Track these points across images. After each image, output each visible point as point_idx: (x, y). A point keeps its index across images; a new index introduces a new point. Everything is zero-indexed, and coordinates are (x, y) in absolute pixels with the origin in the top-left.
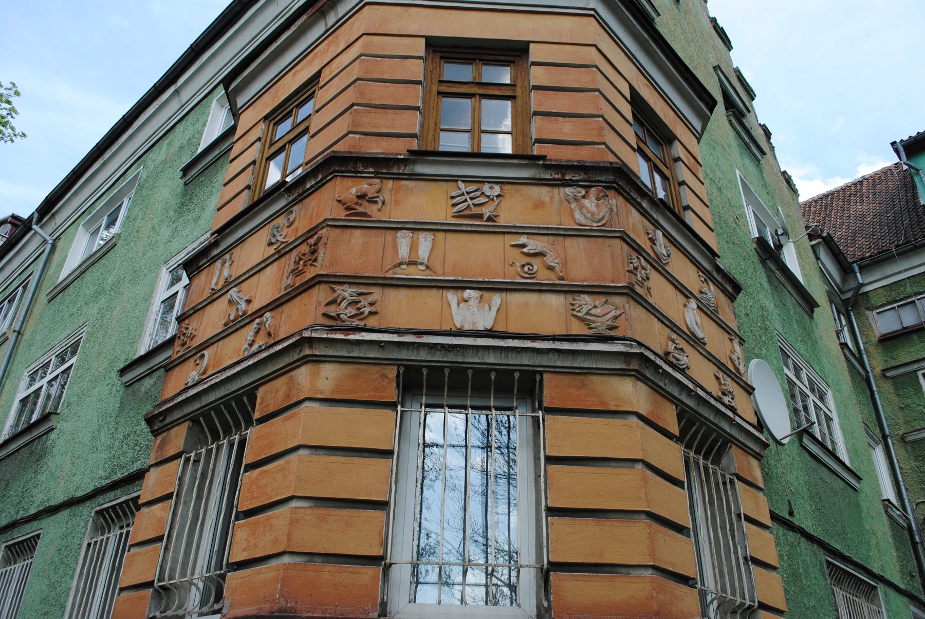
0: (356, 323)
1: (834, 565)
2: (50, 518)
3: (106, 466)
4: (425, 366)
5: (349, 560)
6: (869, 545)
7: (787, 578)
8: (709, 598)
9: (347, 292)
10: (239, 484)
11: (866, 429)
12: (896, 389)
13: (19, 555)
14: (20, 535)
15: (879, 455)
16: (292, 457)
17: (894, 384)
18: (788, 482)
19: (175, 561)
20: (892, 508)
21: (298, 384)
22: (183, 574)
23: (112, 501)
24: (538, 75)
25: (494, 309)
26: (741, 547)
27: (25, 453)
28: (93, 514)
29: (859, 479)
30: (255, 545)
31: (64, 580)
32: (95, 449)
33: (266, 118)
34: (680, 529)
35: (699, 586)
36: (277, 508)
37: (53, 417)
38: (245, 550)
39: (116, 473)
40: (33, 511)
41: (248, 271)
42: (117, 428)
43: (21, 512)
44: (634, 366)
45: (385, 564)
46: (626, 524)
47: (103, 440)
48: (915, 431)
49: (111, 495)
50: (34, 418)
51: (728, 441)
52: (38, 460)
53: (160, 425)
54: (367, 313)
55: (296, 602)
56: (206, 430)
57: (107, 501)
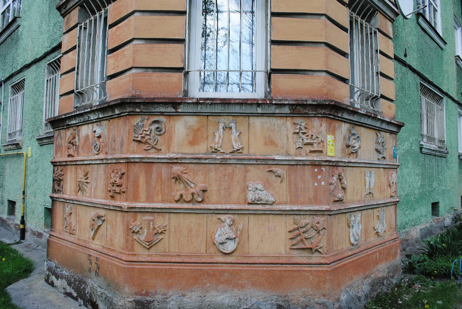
1: (424, 85)
2: (27, 70)
3: (48, 41)
5: (166, 70)
6: (444, 77)
8: (356, 90)
10: (107, 36)
11: (454, 18)
13: (19, 91)
14: (16, 79)
16: (132, 18)
18: (407, 41)
19: (82, 80)
20: (459, 60)
22: (87, 85)
23: (54, 58)
26: (376, 67)
27: (9, 40)
28: (46, 66)
29: (445, 43)
30: (118, 66)
31: (39, 98)
32: (41, 33)
34: (344, 54)
35: (350, 83)
36: (127, 45)
37: (18, 19)
38: (113, 69)
39: (53, 44)
40: (19, 68)
42: (50, 21)
43: (14, 69)
45: (185, 72)
46: (314, 49)
47: (44, 28)
49: (53, 55)
50: (10, 21)
51: (376, 10)
52: (16, 43)
53: (65, 10)
55: (141, 92)
56: (88, 10)
57: (52, 58)
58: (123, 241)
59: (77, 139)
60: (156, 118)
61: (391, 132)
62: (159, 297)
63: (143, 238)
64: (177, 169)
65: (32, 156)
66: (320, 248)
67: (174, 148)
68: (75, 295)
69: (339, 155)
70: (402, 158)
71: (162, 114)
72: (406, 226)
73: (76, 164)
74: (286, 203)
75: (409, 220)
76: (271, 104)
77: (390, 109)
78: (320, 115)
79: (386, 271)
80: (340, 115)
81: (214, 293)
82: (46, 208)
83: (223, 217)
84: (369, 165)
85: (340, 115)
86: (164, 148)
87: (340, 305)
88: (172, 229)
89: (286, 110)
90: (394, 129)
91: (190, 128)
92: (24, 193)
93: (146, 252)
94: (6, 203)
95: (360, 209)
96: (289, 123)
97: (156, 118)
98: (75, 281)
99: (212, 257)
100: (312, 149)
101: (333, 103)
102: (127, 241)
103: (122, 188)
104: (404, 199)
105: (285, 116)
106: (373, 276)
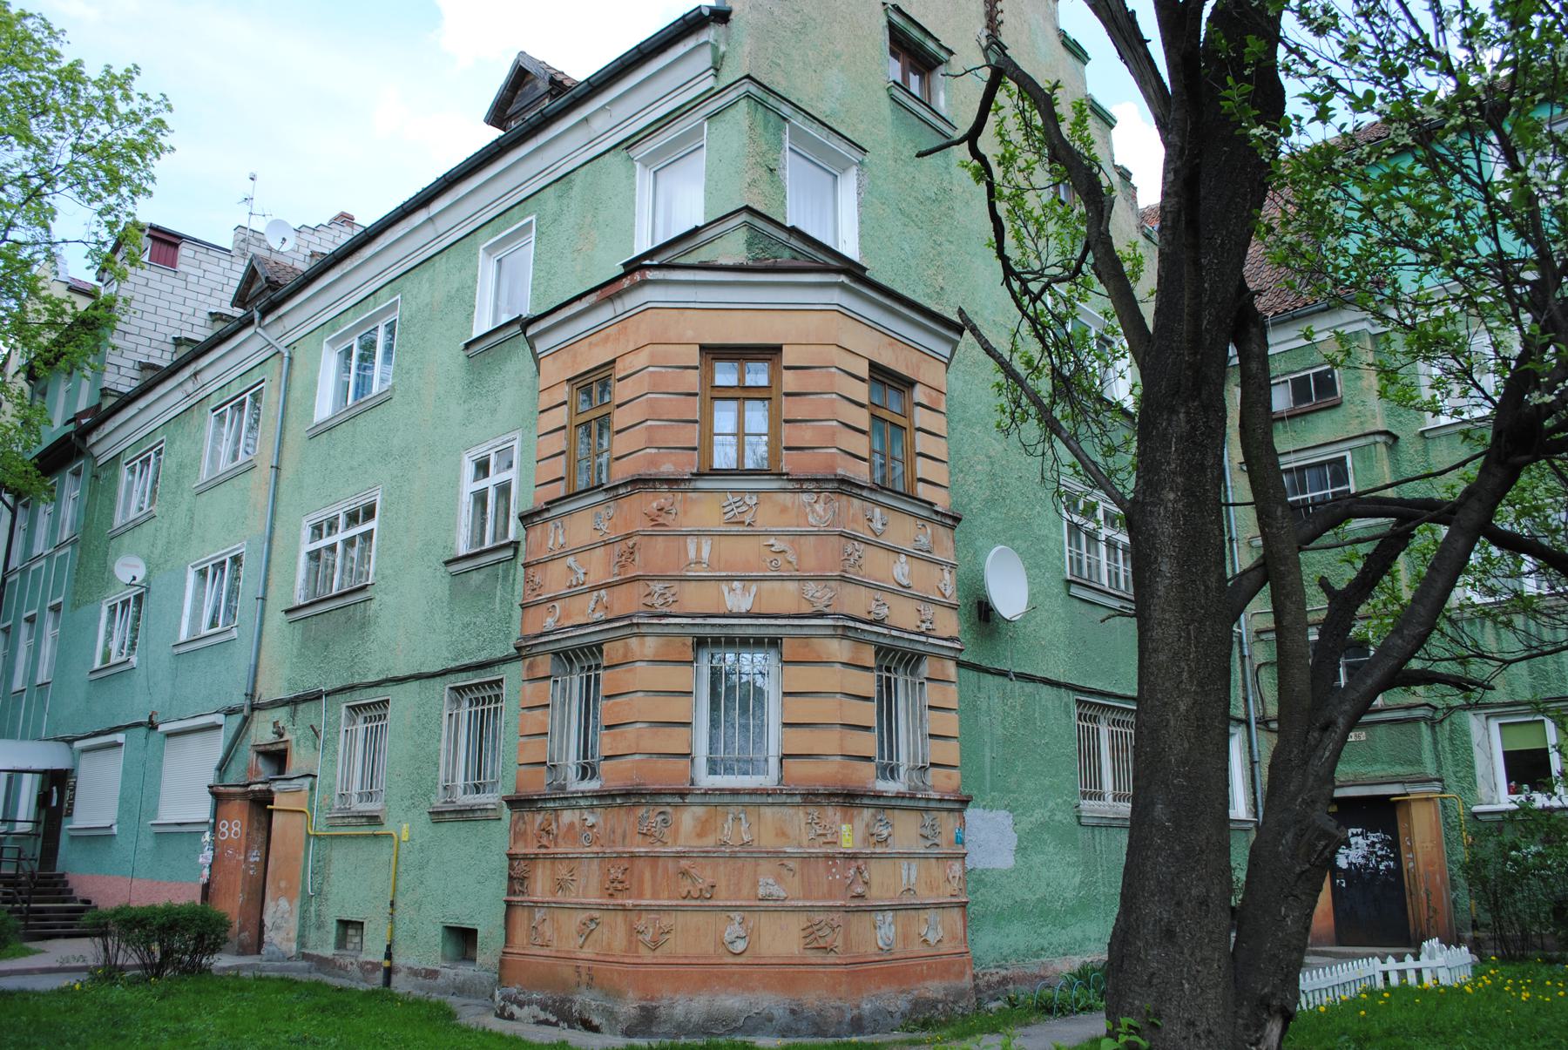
0: (665, 610)
9: (657, 587)
24: (790, 381)
33: (568, 380)
44: (840, 631)
49: (464, 675)
58: (625, 943)
59: (554, 826)
60: (662, 809)
62: (665, 1002)
63: (648, 938)
64: (684, 863)
65: (411, 839)
67: (682, 841)
68: (553, 1019)
71: (668, 804)
73: (554, 858)
74: (798, 899)
75: (1051, 944)
76: (781, 794)
81: (723, 996)
82: (447, 928)
83: (732, 915)
84: (909, 856)
86: (670, 841)
88: (679, 929)
89: (798, 799)
92: (392, 904)
93: (652, 954)
94: (333, 927)
95: (894, 909)
96: (801, 812)
97: (662, 809)
98: (554, 1001)
99: (721, 957)
102: (630, 942)
105: (793, 805)
106: (916, 992)
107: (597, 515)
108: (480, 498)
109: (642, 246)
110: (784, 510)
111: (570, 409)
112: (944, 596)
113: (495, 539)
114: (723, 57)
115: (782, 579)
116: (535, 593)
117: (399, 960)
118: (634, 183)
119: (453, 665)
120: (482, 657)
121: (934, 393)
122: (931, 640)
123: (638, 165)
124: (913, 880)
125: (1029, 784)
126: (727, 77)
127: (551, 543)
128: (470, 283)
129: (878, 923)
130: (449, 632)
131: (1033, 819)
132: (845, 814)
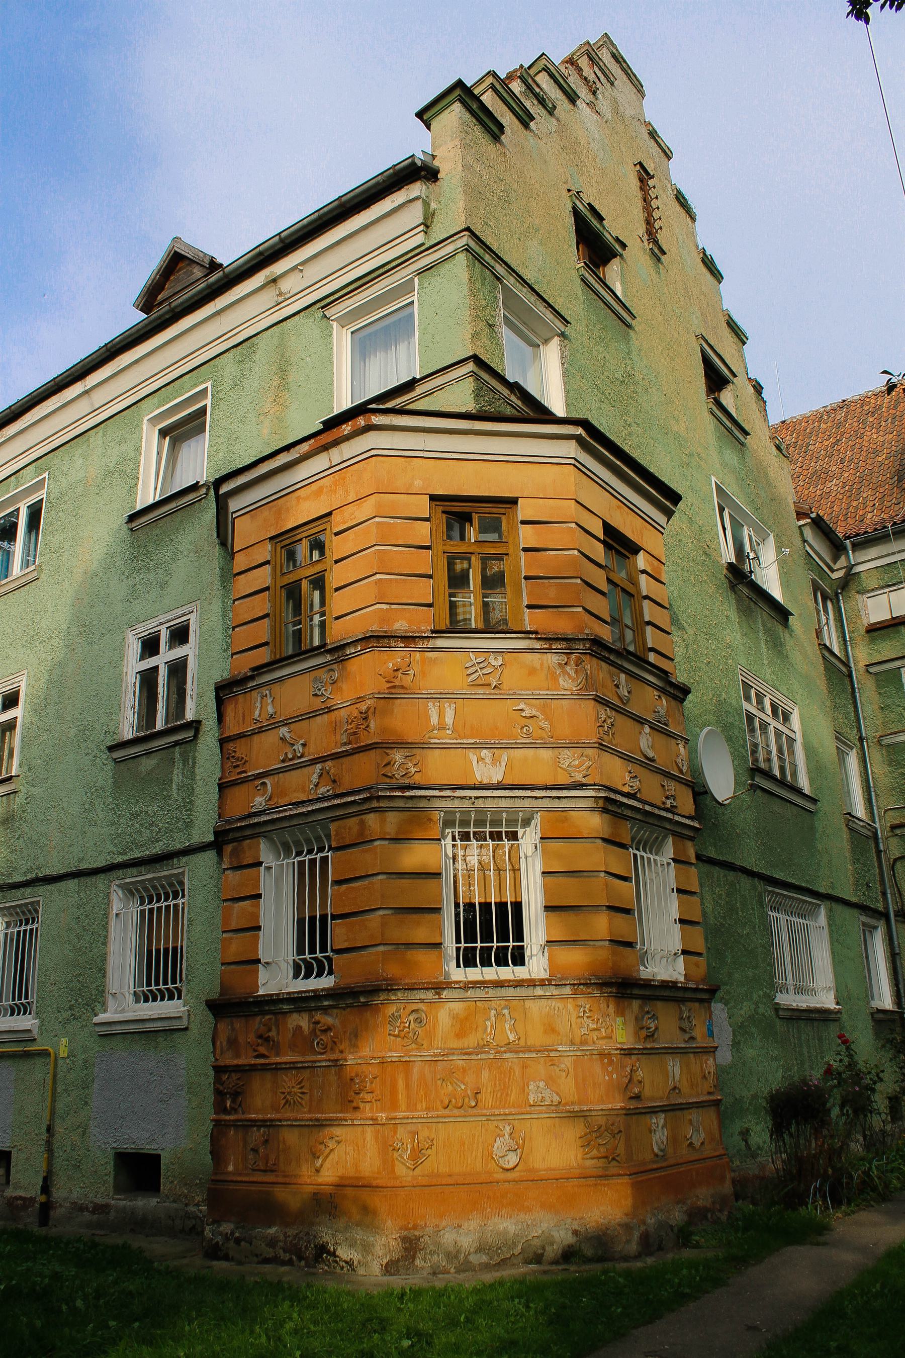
4: (459, 811)
7: (724, 913)
12: (878, 686)
15: (852, 761)
17: (877, 680)
21: (370, 826)
25: (504, 764)
33: (271, 539)
38: (345, 941)
41: (297, 716)
48: (891, 734)
54: (413, 772)
61: (701, 1001)
66: (617, 1156)
69: (632, 1039)
70: (739, 1032)
71: (422, 1001)
72: (759, 1152)
73: (277, 1068)
77: (698, 967)
78: (606, 995)
79: (710, 1200)
80: (628, 992)
81: (496, 1220)
85: (628, 992)
87: (646, 1229)
89: (567, 990)
90: (705, 996)
91: (454, 1017)
92: (49, 1129)
95: (663, 1109)
97: (415, 1007)
100: (599, 1036)
101: (620, 980)
103: (374, 1095)
104: (750, 1104)
105: (562, 998)
107: (316, 680)
108: (148, 679)
109: (344, 403)
110: (532, 671)
111: (274, 570)
112: (681, 771)
113: (167, 723)
114: (433, 214)
115: (534, 746)
116: (239, 770)
117: (59, 1193)
118: (331, 343)
119: (119, 859)
120: (157, 849)
121: (656, 563)
122: (677, 818)
123: (335, 324)
124: (677, 1077)
125: (737, 976)
126: (438, 233)
127: (257, 713)
128: (132, 455)
129: (654, 1127)
130: (113, 823)
131: (742, 1012)
132: (618, 1005)
